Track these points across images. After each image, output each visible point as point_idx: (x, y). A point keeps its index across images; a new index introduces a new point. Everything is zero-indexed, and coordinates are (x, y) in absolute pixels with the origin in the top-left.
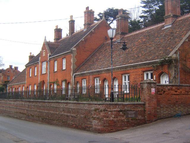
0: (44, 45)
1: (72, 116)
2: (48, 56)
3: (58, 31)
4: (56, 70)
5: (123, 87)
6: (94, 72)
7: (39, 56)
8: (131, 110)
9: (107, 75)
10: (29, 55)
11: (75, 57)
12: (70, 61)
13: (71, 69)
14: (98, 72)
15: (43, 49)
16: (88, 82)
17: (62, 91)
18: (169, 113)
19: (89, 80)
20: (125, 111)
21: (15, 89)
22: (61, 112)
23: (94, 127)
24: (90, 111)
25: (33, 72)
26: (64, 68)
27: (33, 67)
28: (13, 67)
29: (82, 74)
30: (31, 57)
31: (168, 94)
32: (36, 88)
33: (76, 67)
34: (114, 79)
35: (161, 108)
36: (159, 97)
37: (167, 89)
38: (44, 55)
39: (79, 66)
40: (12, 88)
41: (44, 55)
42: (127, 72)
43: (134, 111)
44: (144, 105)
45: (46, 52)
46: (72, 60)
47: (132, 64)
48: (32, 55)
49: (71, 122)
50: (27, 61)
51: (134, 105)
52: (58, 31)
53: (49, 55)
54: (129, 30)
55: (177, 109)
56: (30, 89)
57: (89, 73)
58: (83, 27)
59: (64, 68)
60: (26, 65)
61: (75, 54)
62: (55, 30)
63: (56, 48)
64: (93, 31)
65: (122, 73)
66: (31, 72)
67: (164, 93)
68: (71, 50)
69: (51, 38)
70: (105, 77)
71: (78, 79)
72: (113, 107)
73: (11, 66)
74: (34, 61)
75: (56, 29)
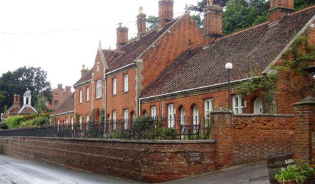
0: (98, 55)
1: (119, 161)
2: (104, 71)
3: (122, 31)
4: (115, 93)
5: (169, 118)
6: (167, 96)
7: (91, 71)
8: (195, 152)
9: (181, 101)
10: (82, 69)
11: (142, 73)
12: (134, 79)
13: (134, 91)
14: (172, 95)
15: (97, 60)
16: (159, 110)
17: (123, 123)
18: (254, 155)
19: (160, 107)
20: (184, 152)
21: (61, 121)
22: (106, 154)
23: (144, 174)
24: (139, 153)
25: (85, 96)
26: (126, 90)
27: (122, 75)
28: (63, 87)
29: (151, 99)
30: (84, 72)
31: (251, 128)
32: (88, 119)
33: (142, 88)
34: (193, 106)
35: (241, 147)
36: (238, 132)
37: (249, 121)
38: (98, 70)
39: (151, 86)
40: (56, 120)
41: (98, 70)
42: (210, 95)
43: (199, 152)
44: (215, 143)
45: (101, 64)
46: (136, 78)
47: (214, 85)
48: (86, 69)
49: (117, 169)
50: (79, 77)
51: (199, 143)
52: (122, 31)
53: (104, 69)
54: (52, 96)
55: (266, 149)
56: (115, 118)
57: (160, 97)
58: (136, 36)
59: (126, 90)
60: (75, 84)
61: (141, 68)
62: (117, 29)
63: (118, 59)
64: (169, 31)
65: (204, 97)
66: (81, 95)
67: (245, 127)
68: (134, 62)
69: (112, 44)
70: (181, 103)
71: (146, 106)
72: (168, 147)
73: (60, 86)
74: (87, 75)
75: (119, 28)
